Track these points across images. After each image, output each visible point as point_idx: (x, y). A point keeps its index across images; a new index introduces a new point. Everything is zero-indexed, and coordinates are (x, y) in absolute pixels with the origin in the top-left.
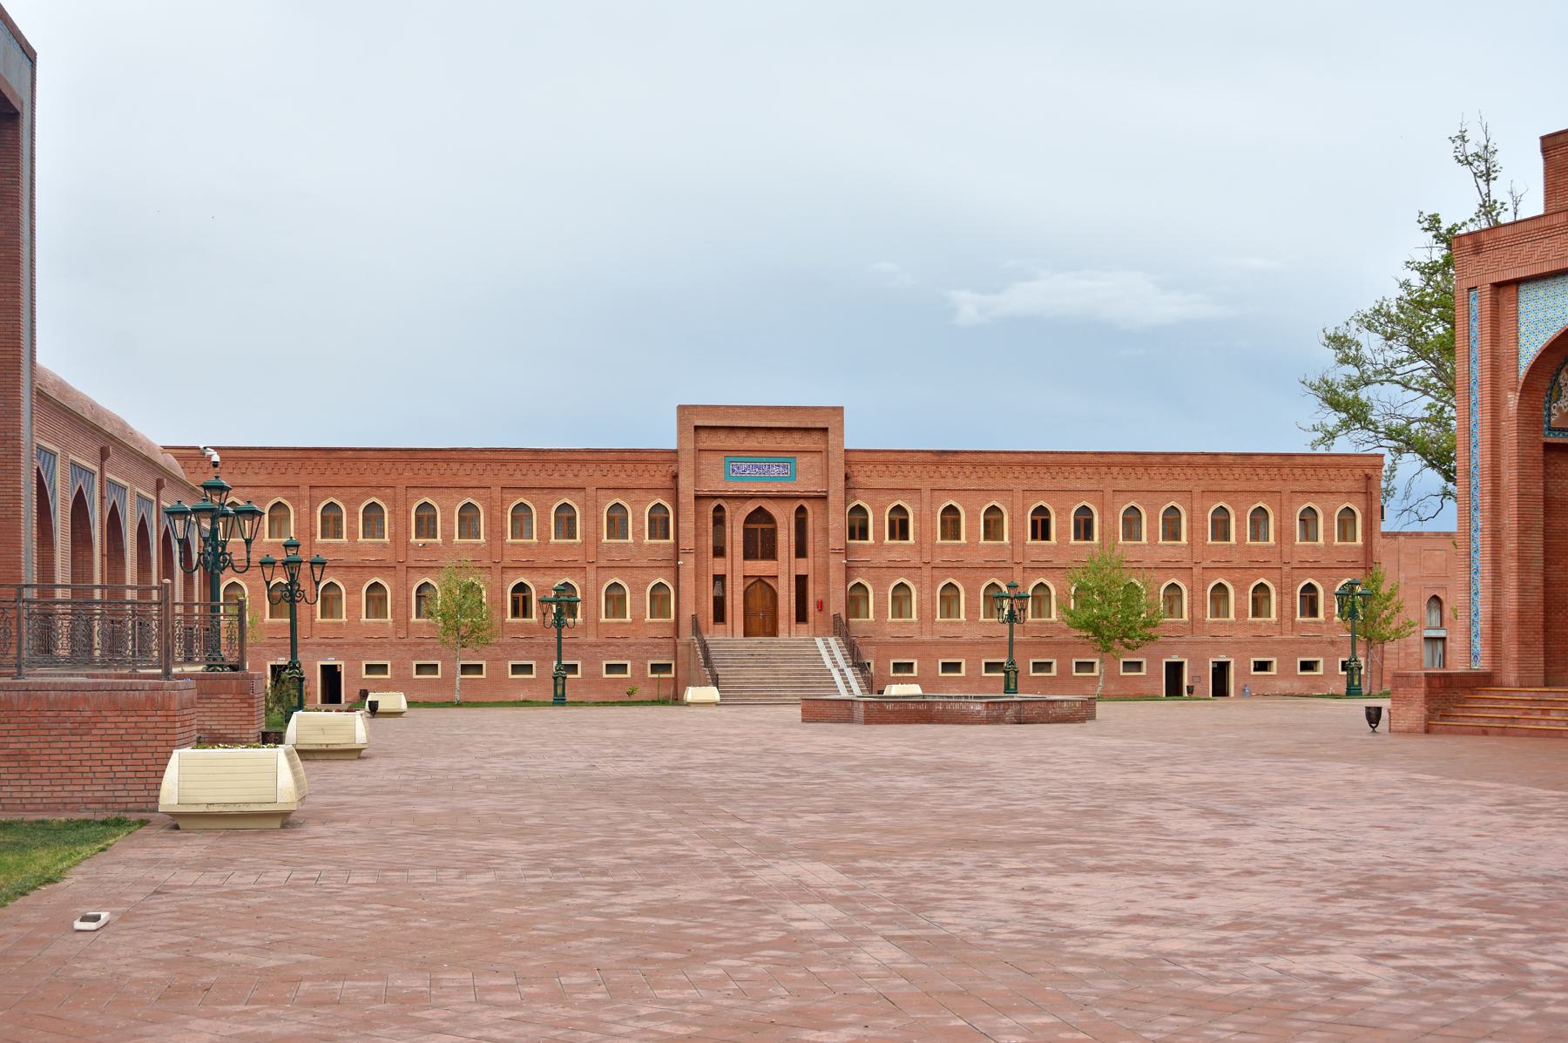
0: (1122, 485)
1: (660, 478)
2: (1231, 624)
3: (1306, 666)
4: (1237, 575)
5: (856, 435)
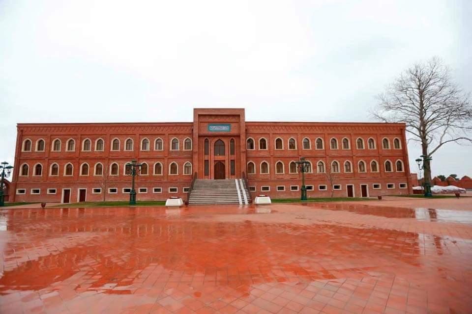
0: (331, 132)
2: (366, 173)
3: (389, 186)
4: (366, 159)
5: (249, 118)
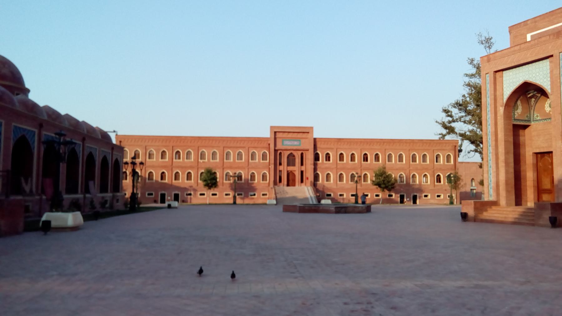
1: (266, 145)
3: (439, 196)
